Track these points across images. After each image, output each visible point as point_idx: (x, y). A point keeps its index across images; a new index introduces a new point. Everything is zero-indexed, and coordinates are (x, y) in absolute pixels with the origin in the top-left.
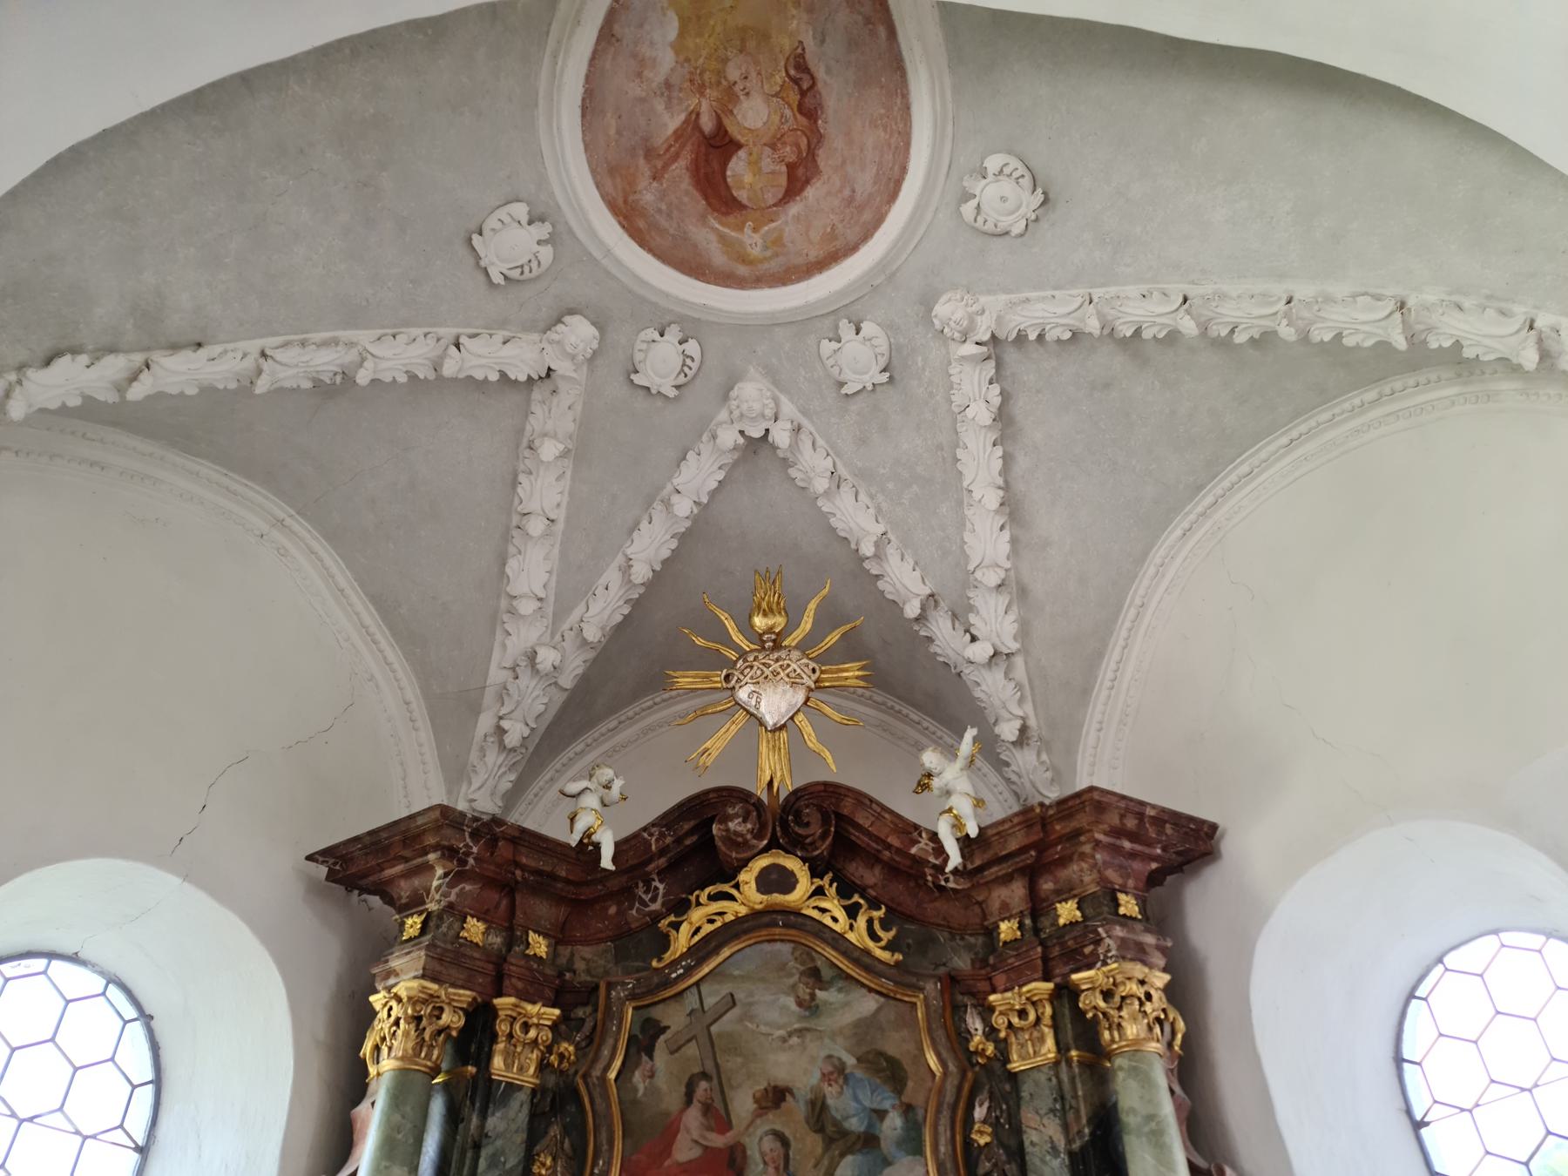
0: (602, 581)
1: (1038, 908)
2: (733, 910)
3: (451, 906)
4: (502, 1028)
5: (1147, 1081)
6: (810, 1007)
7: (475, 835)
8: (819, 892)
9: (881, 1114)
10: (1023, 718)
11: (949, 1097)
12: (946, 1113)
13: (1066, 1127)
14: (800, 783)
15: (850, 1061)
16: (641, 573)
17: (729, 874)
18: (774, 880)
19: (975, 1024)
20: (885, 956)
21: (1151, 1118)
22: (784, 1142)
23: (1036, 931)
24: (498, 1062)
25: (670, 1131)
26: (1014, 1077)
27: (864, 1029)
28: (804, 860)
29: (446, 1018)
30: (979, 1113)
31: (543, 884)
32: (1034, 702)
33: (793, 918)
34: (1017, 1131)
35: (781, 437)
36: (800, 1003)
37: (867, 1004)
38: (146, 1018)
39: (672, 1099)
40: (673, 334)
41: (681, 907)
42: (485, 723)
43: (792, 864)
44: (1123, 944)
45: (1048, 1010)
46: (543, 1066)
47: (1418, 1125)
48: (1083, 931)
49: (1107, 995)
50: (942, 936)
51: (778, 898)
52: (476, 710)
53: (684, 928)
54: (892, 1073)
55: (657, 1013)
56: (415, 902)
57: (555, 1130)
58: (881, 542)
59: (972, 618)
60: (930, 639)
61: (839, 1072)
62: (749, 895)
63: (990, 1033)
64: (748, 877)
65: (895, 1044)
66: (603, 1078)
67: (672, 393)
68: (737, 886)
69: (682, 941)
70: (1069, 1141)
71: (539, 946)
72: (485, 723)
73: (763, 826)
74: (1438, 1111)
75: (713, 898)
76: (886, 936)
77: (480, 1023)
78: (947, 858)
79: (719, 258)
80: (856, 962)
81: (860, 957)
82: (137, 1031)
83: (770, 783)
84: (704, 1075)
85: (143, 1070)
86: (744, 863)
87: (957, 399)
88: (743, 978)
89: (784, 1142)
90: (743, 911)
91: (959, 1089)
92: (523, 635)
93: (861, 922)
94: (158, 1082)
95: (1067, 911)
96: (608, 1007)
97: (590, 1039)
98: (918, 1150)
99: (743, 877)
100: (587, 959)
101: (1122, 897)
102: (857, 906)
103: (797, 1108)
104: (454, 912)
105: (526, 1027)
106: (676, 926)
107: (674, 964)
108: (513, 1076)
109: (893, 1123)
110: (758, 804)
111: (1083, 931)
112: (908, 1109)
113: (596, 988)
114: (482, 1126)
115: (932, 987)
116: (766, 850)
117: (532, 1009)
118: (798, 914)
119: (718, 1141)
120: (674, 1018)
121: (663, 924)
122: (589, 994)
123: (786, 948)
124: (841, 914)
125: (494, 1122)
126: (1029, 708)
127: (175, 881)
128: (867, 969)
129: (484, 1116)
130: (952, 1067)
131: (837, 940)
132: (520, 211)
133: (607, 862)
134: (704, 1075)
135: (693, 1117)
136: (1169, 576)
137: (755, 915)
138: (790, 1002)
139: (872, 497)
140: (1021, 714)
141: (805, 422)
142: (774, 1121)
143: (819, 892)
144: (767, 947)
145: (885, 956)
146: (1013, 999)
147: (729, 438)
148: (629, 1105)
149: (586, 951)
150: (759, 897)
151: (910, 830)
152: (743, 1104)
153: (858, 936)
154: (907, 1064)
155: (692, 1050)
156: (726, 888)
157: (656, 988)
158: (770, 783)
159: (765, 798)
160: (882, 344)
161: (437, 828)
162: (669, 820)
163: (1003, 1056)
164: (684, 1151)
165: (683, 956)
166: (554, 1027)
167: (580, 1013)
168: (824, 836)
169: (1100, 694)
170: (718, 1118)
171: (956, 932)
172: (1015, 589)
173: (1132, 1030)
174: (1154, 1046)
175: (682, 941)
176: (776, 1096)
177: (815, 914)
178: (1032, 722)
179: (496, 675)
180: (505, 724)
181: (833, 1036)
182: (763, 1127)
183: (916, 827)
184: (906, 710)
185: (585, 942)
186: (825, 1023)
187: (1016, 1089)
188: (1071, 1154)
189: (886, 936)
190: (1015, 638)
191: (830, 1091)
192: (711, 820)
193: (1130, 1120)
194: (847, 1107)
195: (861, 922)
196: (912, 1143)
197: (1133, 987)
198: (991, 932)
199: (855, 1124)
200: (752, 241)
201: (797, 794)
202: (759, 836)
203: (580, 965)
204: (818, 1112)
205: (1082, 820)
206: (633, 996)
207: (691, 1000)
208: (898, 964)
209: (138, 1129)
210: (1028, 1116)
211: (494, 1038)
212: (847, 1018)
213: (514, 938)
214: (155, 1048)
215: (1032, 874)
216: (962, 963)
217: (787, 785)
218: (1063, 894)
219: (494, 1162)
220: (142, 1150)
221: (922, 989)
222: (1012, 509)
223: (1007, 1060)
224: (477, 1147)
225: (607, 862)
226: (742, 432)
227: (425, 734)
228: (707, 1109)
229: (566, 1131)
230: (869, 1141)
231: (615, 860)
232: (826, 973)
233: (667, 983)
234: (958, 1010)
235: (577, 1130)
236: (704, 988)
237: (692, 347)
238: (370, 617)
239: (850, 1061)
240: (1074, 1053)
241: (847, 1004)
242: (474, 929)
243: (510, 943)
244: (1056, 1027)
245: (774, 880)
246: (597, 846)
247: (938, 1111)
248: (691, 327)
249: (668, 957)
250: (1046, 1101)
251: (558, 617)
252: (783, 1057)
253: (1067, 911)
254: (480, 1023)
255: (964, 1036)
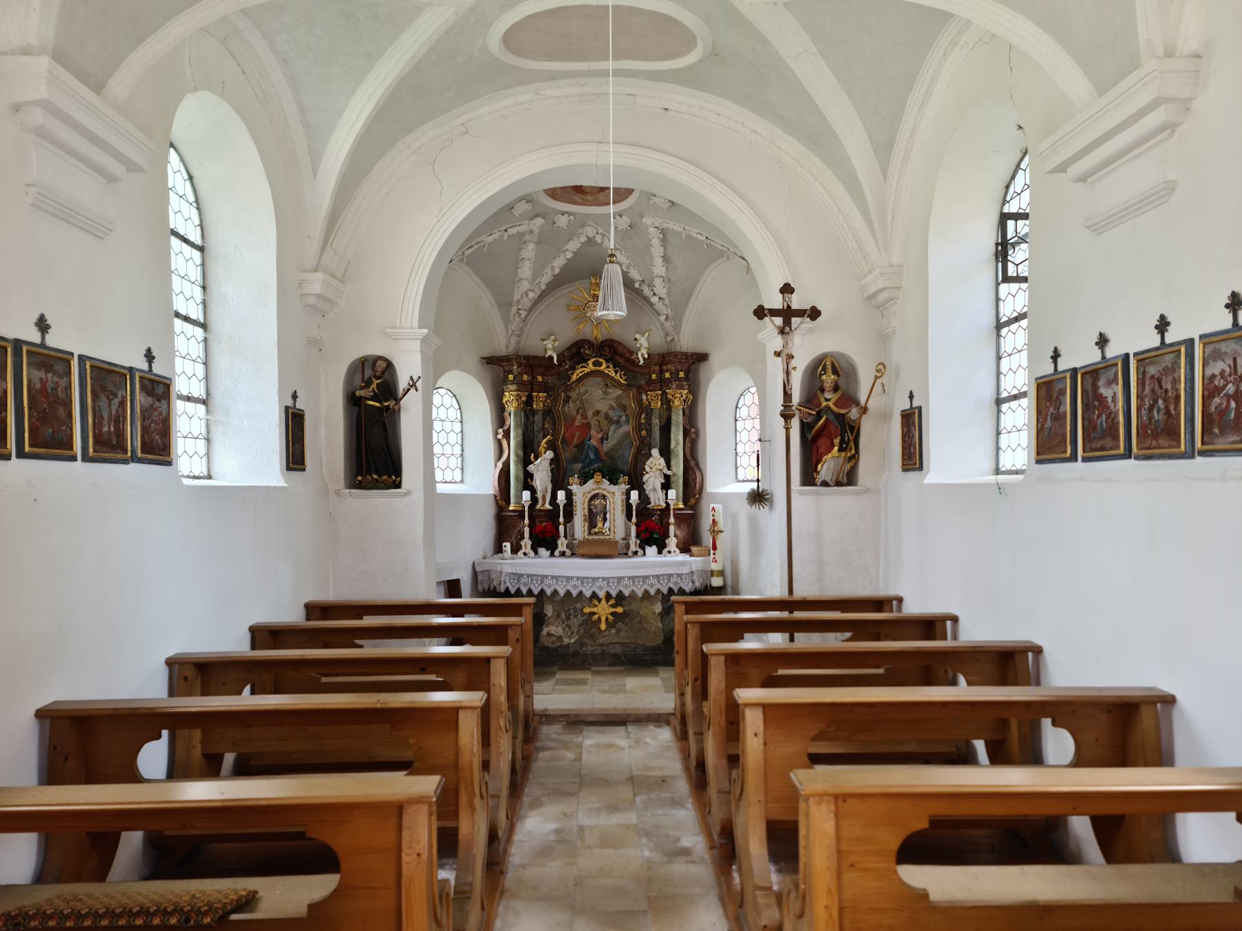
0: (545, 271)
1: (661, 372)
2: (586, 370)
3: (520, 373)
4: (535, 399)
5: (678, 415)
6: (606, 393)
7: (524, 359)
8: (608, 367)
9: (621, 417)
10: (667, 315)
11: (636, 414)
12: (634, 419)
13: (660, 421)
14: (604, 339)
15: (615, 405)
16: (557, 271)
17: (586, 361)
18: (597, 364)
19: (644, 397)
20: (624, 382)
21: (677, 422)
22: (599, 422)
23: (661, 377)
24: (535, 406)
25: (574, 420)
26: (652, 409)
27: (618, 398)
28: (604, 359)
29: (523, 399)
30: (643, 416)
31: (539, 365)
32: (671, 308)
33: (601, 372)
34: (651, 420)
35: (599, 239)
36: (603, 392)
37: (620, 392)
38: (455, 396)
39: (574, 413)
40: (566, 215)
41: (573, 368)
42: (514, 309)
43: (601, 360)
44: (677, 385)
45: (660, 397)
46: (544, 405)
47: (736, 420)
48: (669, 381)
49: (673, 396)
50: (639, 375)
51: (598, 368)
52: (511, 305)
53: (575, 374)
54: (624, 408)
55: (569, 394)
56: (511, 372)
57: (548, 418)
58: (629, 265)
59: (654, 288)
60: (643, 291)
61: (612, 408)
62: (591, 367)
63: (647, 400)
64: (590, 362)
65: (625, 401)
66: (558, 410)
67: (566, 228)
68: (587, 364)
69: (574, 377)
70: (660, 423)
71: (540, 379)
72: (514, 309)
73: (594, 350)
74: (740, 419)
75: (581, 367)
76: (624, 378)
77: (530, 400)
78: (640, 361)
79: (580, 201)
80: (617, 383)
81: (618, 382)
82: (454, 398)
83: (596, 338)
84: (581, 408)
85: (457, 407)
86: (589, 360)
87: (650, 236)
88: (589, 386)
89: (599, 422)
90: (589, 370)
91: (638, 412)
92: (525, 285)
93: (618, 375)
94: (460, 408)
95: (667, 375)
96: (558, 393)
97: (554, 399)
98: (629, 424)
99: (589, 362)
100: (551, 380)
101: (680, 373)
102: (617, 371)
103: (602, 415)
104: (521, 374)
105: (539, 398)
106: (573, 374)
107: (573, 383)
108: (538, 408)
109: (624, 418)
110: (593, 344)
111: (669, 381)
112: (627, 416)
113: (554, 387)
114: (533, 419)
115: (634, 390)
116: (595, 357)
117: (541, 394)
118: (603, 372)
119: (585, 421)
120: (573, 395)
121: (569, 373)
122: (552, 389)
123: (599, 379)
124: (614, 373)
125: (536, 418)
126: (669, 310)
127: (459, 372)
128: (620, 385)
129: (533, 417)
130: (638, 409)
131: (612, 378)
132: (525, 201)
133: (555, 362)
134: (581, 408)
135: (579, 416)
136: (712, 274)
137: (592, 372)
138: (601, 392)
139: (626, 253)
140: (666, 313)
141: (606, 234)
142: (596, 418)
143: (608, 367)
144: (595, 378)
145: (624, 382)
146: (653, 394)
147: (583, 239)
148: (564, 414)
149: (551, 378)
150: (593, 368)
151: (632, 353)
152: (590, 414)
153: (618, 377)
154: (627, 406)
155: (578, 402)
156: (584, 365)
157: (569, 388)
158: (596, 338)
159: (594, 342)
160: (629, 222)
161: (516, 358)
162: (569, 348)
163: (650, 404)
164: (577, 423)
165: (575, 381)
166: (545, 397)
167: (551, 393)
168: (610, 353)
169: (691, 304)
170: (584, 416)
171: (642, 374)
172: (667, 280)
173: (676, 403)
174: (681, 407)
175: (574, 377)
176: (598, 412)
177: (607, 372)
178: (670, 314)
179: (516, 298)
180: (521, 312)
181: (611, 400)
182: (594, 419)
183: (633, 352)
184: (637, 296)
185: (550, 375)
186: (609, 397)
187: (652, 412)
188: (660, 426)
189: (624, 378)
190: (666, 294)
191: (610, 412)
192: (581, 348)
193: (673, 422)
194: (612, 414)
195: (618, 375)
196: (627, 422)
197: (677, 395)
198: (651, 375)
199: (615, 419)
200: (589, 197)
201: (602, 342)
202: (593, 353)
203: (549, 382)
204: (607, 416)
205: (672, 358)
206: (563, 391)
207: (577, 391)
208: (627, 385)
209: (459, 418)
210: (653, 418)
211: (533, 401)
212: (614, 395)
213: (534, 378)
214: (458, 401)
215: (661, 365)
216: (643, 382)
217: (600, 338)
218: (667, 371)
219: (537, 426)
220: (461, 422)
221: (632, 390)
222: (665, 258)
223: (650, 405)
224: (533, 423)
225: (555, 362)
226: (587, 236)
227: (496, 310)
228: (582, 415)
229: (551, 419)
230: (618, 422)
231: (557, 361)
232: (610, 385)
233: (571, 388)
234: (640, 394)
235: (553, 418)
236: (580, 388)
237: (572, 217)
238: (478, 281)
239: (615, 405)
240: (664, 406)
241: (614, 393)
242: (525, 377)
243: (533, 379)
244: (661, 400)
245: (597, 364)
246: (553, 357)
247: (633, 417)
248: (570, 214)
249: (571, 381)
250: (657, 415)
251: (533, 281)
252: (599, 404)
253: (667, 375)
254: (530, 400)
255: (642, 400)
